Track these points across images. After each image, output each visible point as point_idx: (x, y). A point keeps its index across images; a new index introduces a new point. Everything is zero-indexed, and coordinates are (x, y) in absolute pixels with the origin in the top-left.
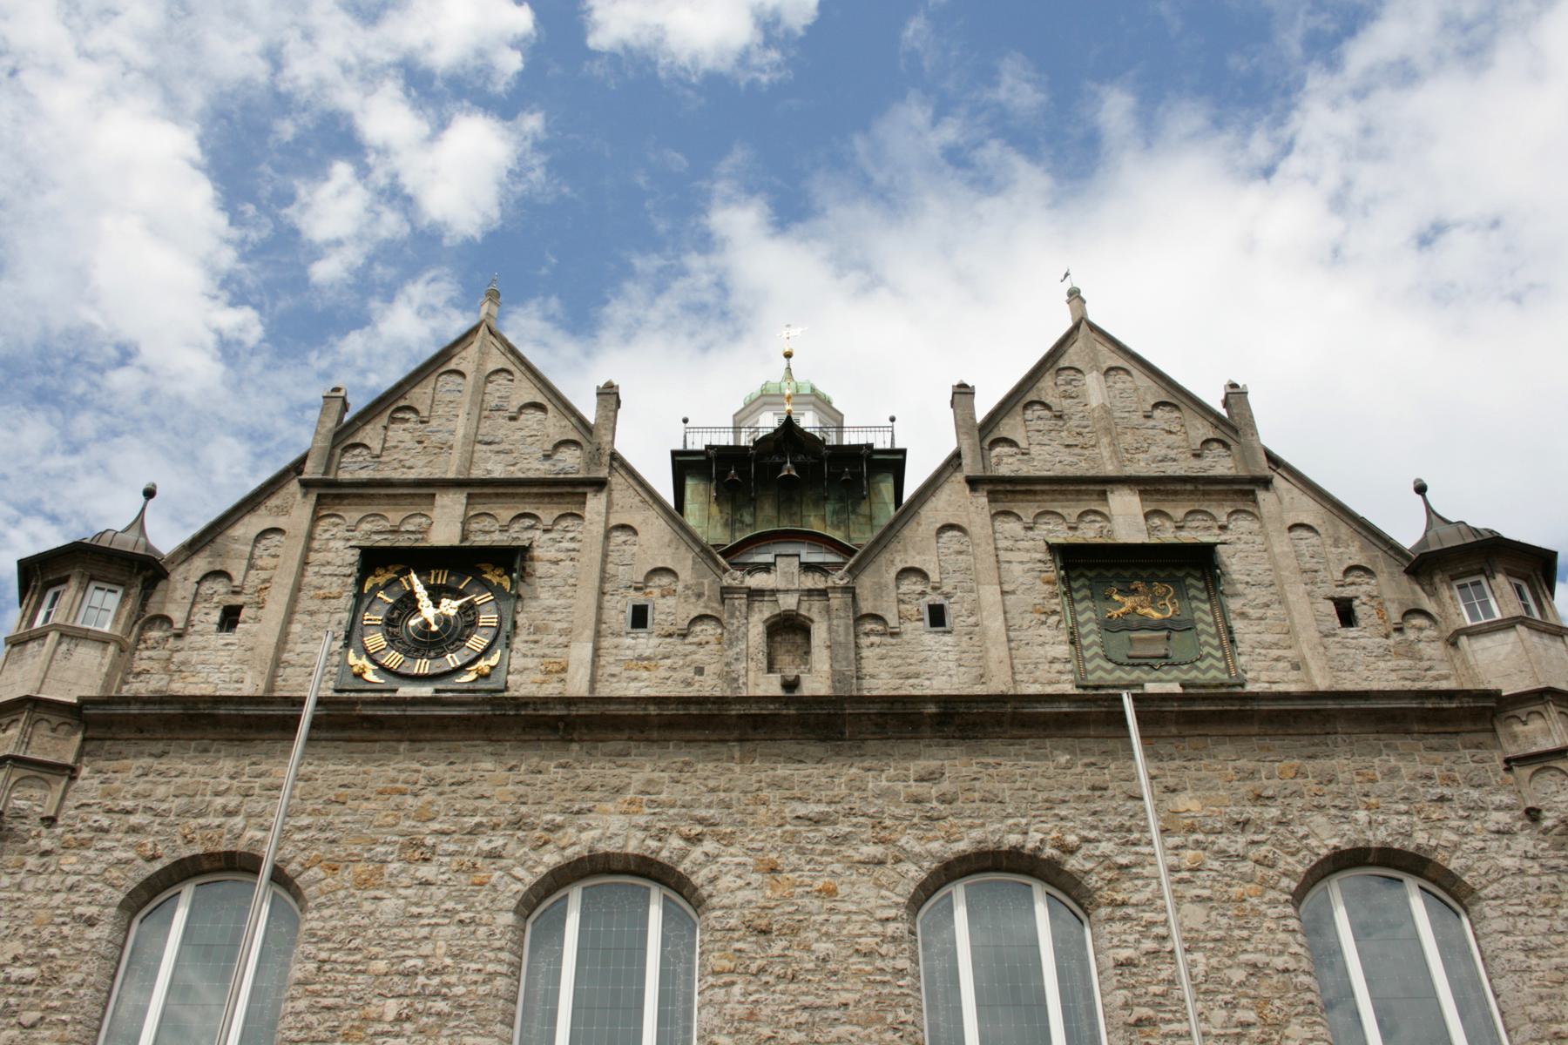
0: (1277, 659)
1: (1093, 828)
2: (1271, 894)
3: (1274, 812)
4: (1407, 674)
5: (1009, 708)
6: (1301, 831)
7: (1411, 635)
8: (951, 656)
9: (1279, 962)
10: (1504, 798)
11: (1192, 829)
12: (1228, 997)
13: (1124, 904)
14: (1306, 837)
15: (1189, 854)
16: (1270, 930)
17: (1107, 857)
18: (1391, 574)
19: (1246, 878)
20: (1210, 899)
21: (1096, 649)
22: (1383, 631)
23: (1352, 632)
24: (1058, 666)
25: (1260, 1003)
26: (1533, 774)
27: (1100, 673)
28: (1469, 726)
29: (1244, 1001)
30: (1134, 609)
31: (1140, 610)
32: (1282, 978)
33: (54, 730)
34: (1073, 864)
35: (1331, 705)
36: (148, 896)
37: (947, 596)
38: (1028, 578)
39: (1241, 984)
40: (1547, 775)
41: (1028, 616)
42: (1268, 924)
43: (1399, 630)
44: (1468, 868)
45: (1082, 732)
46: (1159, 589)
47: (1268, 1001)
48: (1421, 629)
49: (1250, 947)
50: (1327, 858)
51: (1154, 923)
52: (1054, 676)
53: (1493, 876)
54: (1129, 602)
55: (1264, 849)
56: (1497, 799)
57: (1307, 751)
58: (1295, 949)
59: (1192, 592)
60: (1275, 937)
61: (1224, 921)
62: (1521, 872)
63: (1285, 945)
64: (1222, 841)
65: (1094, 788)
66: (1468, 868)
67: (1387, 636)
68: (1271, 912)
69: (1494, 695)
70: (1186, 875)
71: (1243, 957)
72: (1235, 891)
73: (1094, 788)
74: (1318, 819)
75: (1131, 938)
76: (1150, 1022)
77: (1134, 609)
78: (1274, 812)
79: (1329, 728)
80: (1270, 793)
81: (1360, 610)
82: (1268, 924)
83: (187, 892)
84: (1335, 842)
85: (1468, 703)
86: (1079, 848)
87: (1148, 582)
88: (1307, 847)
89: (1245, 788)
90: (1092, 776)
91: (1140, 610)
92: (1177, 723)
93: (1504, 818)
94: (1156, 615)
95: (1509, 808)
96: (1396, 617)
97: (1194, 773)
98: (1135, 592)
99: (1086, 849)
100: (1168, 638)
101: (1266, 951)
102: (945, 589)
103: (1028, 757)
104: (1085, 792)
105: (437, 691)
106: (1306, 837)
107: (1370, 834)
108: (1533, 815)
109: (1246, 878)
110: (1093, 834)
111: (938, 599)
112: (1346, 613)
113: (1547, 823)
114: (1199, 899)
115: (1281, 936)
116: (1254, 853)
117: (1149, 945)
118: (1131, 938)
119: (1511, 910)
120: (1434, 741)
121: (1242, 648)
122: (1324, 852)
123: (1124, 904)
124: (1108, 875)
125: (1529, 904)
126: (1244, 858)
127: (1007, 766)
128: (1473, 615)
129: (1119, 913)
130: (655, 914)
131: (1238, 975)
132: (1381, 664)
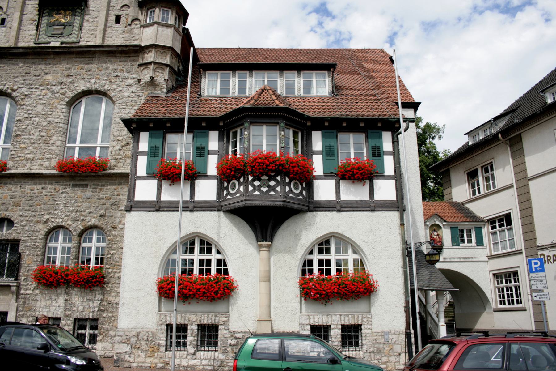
0: (92, 35)
1: (23, 84)
2: (62, 102)
3: (71, 80)
4: (126, 39)
5: (6, 51)
6: (76, 85)
7: (133, 26)
8: (3, 34)
9: (56, 120)
10: (134, 76)
11: (48, 85)
12: (40, 129)
13: (23, 105)
14: (76, 87)
15: (44, 91)
16: (58, 112)
17: (23, 92)
18: (134, 7)
19: (56, 98)
20: (45, 104)
21: (44, 32)
22: (125, 25)
23: (118, 25)
24: (31, 37)
25: (48, 131)
26: (143, 69)
27: (42, 39)
28: (133, 55)
29: (44, 130)
30: (58, 19)
31: (60, 20)
32: (56, 124)
33: (162, 54)
34: (14, 94)
35: (93, 49)
36: (74, 102)
37: (8, 15)
38: (32, 10)
39: (45, 126)
40: (146, 69)
41: (28, 22)
42: (58, 110)
43: (130, 25)
44: (115, 96)
45: (27, 57)
46: (68, 12)
47: (50, 130)
48: (136, 25)
49: (50, 116)
50: (80, 93)
51: (29, 110)
52: (29, 40)
53: (121, 98)
54: (57, 17)
55: (63, 90)
56: (131, 76)
57: (87, 62)
58: (62, 117)
59: (77, 14)
60: (60, 112)
61: (47, 109)
62: (129, 97)
63: (60, 116)
64: (54, 88)
65: (26, 73)
66: (115, 96)
67: (126, 27)
68: (60, 107)
69: (140, 46)
70: (41, 97)
71: (48, 119)
72: (52, 102)
73: (26, 73)
74: (82, 82)
75: (22, 114)
76: (20, 135)
77: (58, 19)
78: (71, 80)
79: (94, 56)
80: (72, 74)
81: (123, 19)
82: (58, 110)
83: (84, 100)
84: (83, 88)
85: (131, 48)
86: (17, 90)
87: (65, 11)
88: (76, 90)
89: (66, 73)
90: (27, 70)
91: (60, 20)
92: (53, 54)
93: (130, 81)
94: (63, 21)
95: (134, 79)
96: (130, 21)
97: (54, 69)
98: (60, 14)
99: (19, 90)
100: (64, 28)
101: (54, 118)
102: (8, 13)
103: (13, 64)
104: (24, 74)
105: (62, 43)
106: (76, 87)
107: (93, 86)
108: (139, 80)
109: (56, 98)
110: (21, 86)
111: (4, 16)
112: (118, 19)
113: (141, 83)
114: (43, 104)
115: (60, 114)
116: (61, 91)
117: (26, 116)
118: (22, 114)
119: (121, 107)
120: (122, 59)
121: (84, 31)
122: (80, 91)
123: (23, 105)
124: (22, 97)
125: (127, 106)
126: (58, 93)
127: (6, 67)
128: (163, 20)
129: (22, 107)
130: (8, 106)
131: (45, 124)
132: (121, 36)
